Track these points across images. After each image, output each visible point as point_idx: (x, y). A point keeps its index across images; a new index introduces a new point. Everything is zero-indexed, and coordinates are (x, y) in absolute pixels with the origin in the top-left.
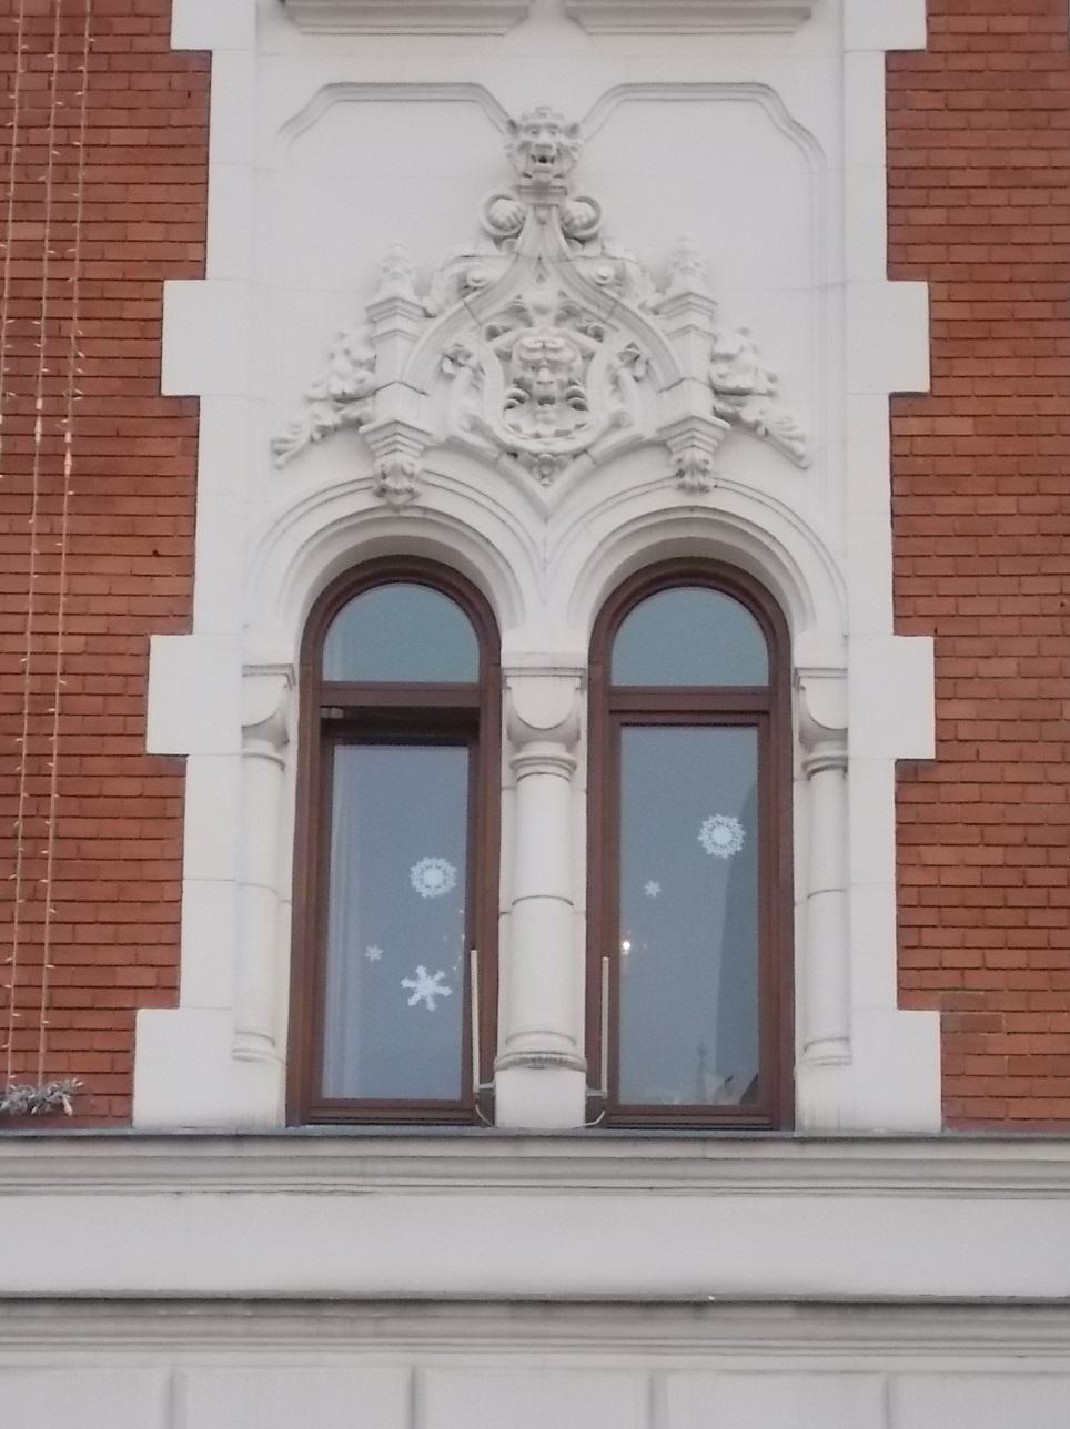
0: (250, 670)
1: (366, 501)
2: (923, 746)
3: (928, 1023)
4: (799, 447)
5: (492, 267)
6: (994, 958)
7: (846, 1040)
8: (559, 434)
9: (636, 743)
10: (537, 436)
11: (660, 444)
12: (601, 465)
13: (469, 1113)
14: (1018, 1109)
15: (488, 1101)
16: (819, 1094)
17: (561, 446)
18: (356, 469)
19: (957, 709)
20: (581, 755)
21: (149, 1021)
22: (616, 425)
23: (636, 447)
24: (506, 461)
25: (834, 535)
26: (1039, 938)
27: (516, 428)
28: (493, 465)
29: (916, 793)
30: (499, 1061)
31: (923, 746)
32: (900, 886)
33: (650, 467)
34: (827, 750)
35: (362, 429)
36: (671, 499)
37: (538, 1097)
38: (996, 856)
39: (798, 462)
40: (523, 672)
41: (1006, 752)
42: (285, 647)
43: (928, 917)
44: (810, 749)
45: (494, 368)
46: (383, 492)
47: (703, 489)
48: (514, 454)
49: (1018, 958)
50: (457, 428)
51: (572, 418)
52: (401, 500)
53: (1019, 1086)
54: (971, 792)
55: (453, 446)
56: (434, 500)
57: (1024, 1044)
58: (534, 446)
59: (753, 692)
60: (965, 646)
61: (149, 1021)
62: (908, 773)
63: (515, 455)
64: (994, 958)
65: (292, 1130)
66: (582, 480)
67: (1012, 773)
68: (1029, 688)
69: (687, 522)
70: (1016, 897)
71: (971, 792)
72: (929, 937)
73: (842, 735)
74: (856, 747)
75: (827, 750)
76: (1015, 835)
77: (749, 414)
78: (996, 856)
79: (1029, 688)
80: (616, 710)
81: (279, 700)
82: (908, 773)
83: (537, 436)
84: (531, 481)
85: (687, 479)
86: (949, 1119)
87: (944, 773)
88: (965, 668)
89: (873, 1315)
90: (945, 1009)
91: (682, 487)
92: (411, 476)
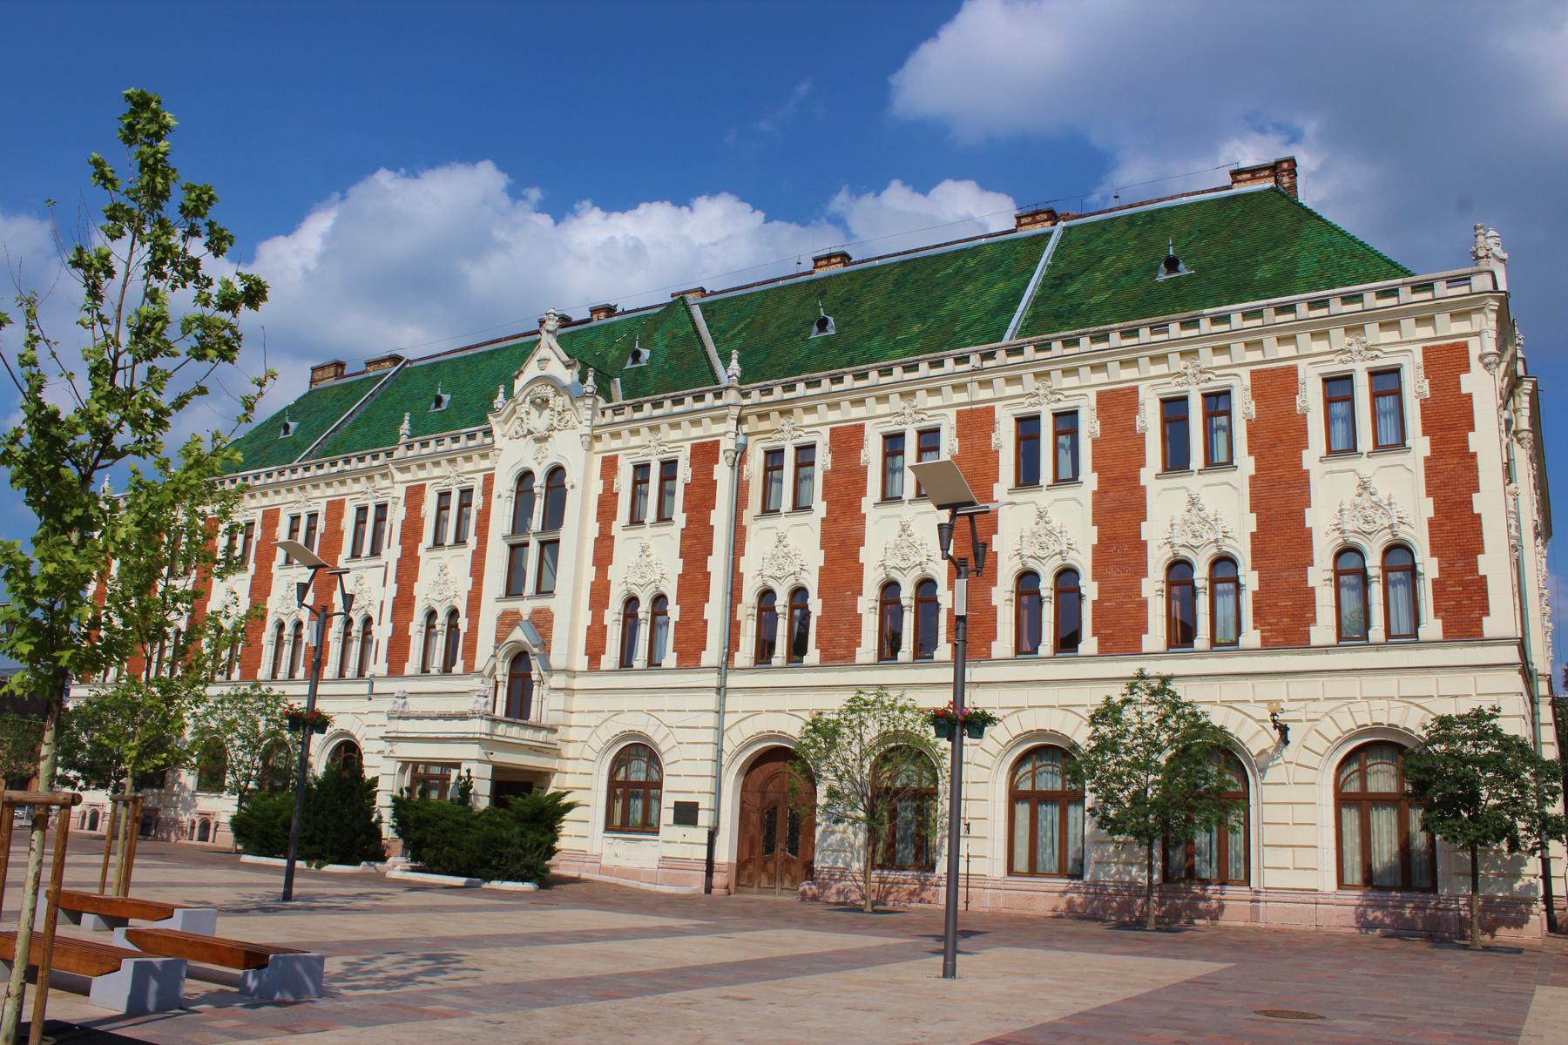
5: (1358, 500)
25: (1242, 551)
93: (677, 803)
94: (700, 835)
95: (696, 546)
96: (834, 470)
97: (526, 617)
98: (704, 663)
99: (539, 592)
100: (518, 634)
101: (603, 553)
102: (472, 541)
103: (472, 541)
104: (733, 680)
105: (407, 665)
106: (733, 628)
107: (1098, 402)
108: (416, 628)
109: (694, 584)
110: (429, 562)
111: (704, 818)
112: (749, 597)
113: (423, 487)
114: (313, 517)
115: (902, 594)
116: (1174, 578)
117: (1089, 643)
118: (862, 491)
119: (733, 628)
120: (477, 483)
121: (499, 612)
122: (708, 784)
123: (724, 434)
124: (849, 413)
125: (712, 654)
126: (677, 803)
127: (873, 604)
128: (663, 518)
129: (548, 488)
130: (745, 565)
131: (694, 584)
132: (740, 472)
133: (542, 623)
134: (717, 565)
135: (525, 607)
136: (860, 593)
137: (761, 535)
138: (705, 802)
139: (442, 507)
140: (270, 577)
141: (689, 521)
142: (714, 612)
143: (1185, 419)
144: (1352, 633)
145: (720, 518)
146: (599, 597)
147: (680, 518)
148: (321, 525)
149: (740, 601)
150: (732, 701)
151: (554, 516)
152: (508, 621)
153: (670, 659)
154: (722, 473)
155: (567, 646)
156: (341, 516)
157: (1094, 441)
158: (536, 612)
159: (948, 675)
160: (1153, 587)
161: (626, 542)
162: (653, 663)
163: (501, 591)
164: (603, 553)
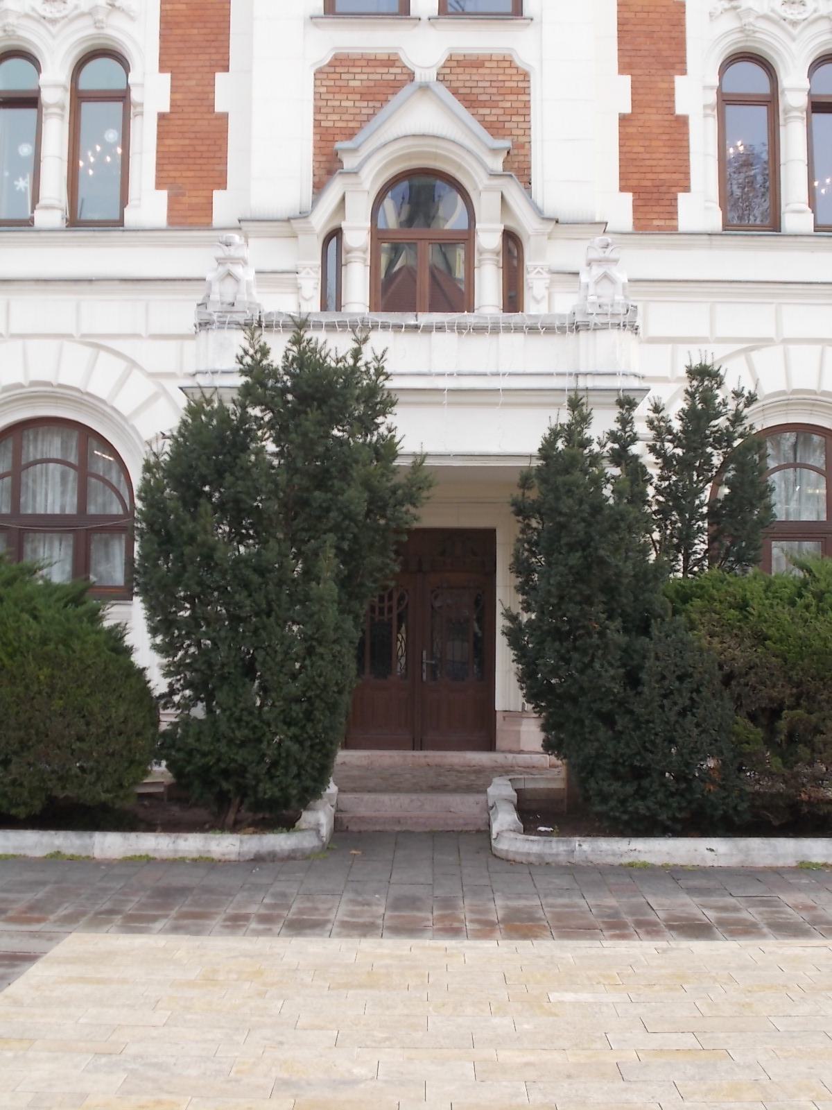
0: (705, 88)
2: (166, 108)
3: (164, 194)
4: (132, 14)
6: (185, 174)
7: (140, 199)
8: (798, 14)
9: (87, 108)
10: (792, 14)
11: (90, 14)
12: (72, 20)
13: (28, 223)
14: (190, 220)
15: (32, 219)
16: (131, 216)
17: (58, 15)
18: (735, 24)
19: (178, 96)
20: (715, 113)
21: (681, 197)
22: (815, 11)
23: (82, 15)
24: (42, 20)
26: (198, 167)
27: (785, 11)
28: (38, 22)
29: (164, 122)
30: (37, 206)
31: (166, 108)
32: (157, 152)
33: (87, 21)
34: (138, 109)
35: (738, 10)
36: (92, 31)
37: (50, 216)
38: (187, 142)
39: (132, 19)
40: (46, 86)
41: (190, 109)
42: (714, 81)
43: (166, 161)
44: (786, 114)
46: (5, 31)
47: (102, 28)
48: (44, 18)
49: (191, 174)
50: (28, 10)
51: (802, 8)
52: (10, 33)
53: (189, 213)
54: (180, 122)
55: (27, 16)
56: (21, 33)
57: (194, 200)
58: (791, 17)
59: (121, 91)
60: (181, 76)
61: (681, 197)
62: (162, 117)
63: (44, 18)
64: (185, 174)
65: (724, 232)
66: (805, 28)
67: (193, 116)
68: (200, 89)
69: (99, 38)
70: (192, 155)
71: (180, 122)
72: (166, 167)
73: (142, 105)
74: (146, 108)
75: (138, 109)
76: (192, 135)
78: (187, 142)
79: (200, 89)
80: (79, 97)
81: (712, 98)
82: (162, 117)
83: (792, 14)
84: (50, 27)
85: (97, 25)
86: (636, 226)
87: (174, 116)
88: (180, 83)
89: (142, 283)
90: (170, 189)
91: (96, 27)
92: (13, 26)
133: (494, 95)
152: (353, 94)
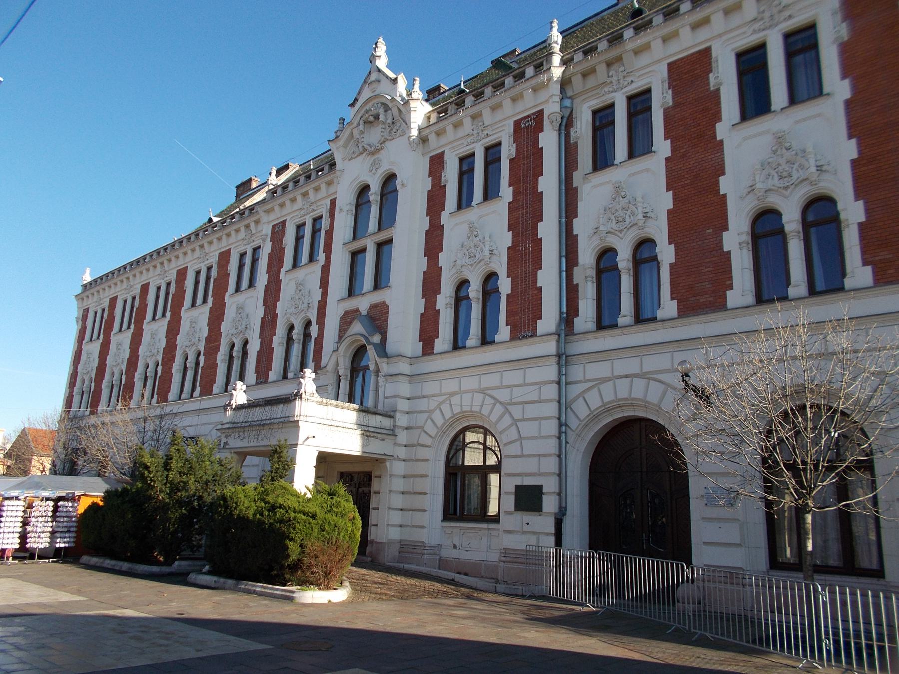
1: (756, 202)
16: (848, 283)
25: (659, 230)
45: (776, 175)
62: (860, 225)
77: (823, 168)
93: (517, 487)
94: (544, 523)
95: (524, 217)
96: (676, 104)
97: (364, 313)
98: (540, 330)
99: (377, 286)
100: (357, 327)
101: (433, 241)
102: (321, 257)
103: (321, 257)
104: (581, 346)
105: (437, 342)
106: (571, 293)
107: (669, 71)
108: (444, 300)
109: (525, 255)
110: (288, 280)
111: (550, 504)
112: (587, 257)
113: (707, 52)
114: (209, 268)
115: (785, 219)
116: (810, 218)
117: (858, 273)
118: (717, 117)
119: (571, 293)
120: (324, 210)
121: (341, 312)
122: (551, 465)
123: (547, 101)
124: (687, 43)
125: (549, 321)
126: (517, 487)
127: (448, 300)
128: (490, 193)
129: (382, 195)
130: (580, 226)
131: (525, 255)
132: (568, 136)
133: (377, 319)
134: (549, 230)
135: (363, 304)
136: (726, 228)
137: (594, 191)
138: (550, 485)
139: (299, 238)
140: (279, 282)
141: (516, 194)
142: (549, 278)
143: (472, 170)
144: (770, 288)
145: (549, 184)
146: (431, 283)
147: (507, 192)
148: (214, 273)
149: (577, 264)
150: (576, 372)
151: (387, 218)
153: (504, 332)
154: (549, 141)
155: (403, 331)
156: (228, 262)
157: (511, 161)
158: (373, 307)
159: (551, 347)
160: (736, 239)
161: (454, 226)
162: (486, 341)
163: (344, 292)
164: (433, 241)
